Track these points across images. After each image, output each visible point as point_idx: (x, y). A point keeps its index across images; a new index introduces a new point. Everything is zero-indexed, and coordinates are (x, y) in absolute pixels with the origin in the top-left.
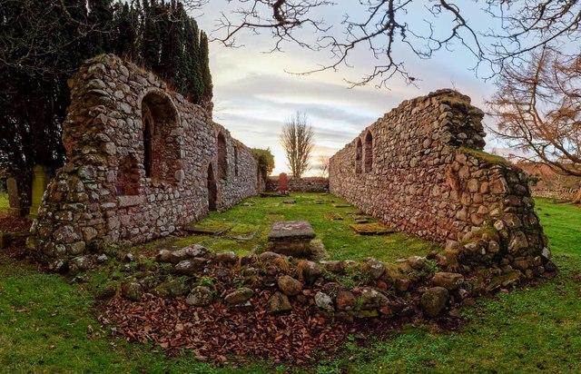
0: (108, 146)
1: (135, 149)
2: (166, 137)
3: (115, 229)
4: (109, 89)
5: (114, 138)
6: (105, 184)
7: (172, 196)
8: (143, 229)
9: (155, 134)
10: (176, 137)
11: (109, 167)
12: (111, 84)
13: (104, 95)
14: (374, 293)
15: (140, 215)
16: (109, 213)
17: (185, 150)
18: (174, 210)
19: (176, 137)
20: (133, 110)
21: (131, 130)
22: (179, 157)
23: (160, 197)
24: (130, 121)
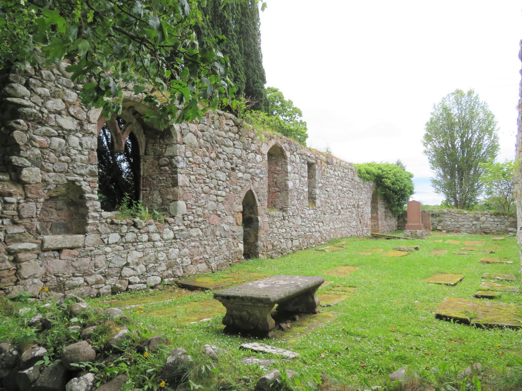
0: (25, 172)
1: (81, 175)
2: (159, 158)
3: (34, 276)
4: (36, 98)
5: (36, 162)
6: (17, 219)
7: (157, 237)
8: (90, 279)
9: (146, 154)
10: (172, 157)
11: (26, 198)
12: (40, 90)
13: (25, 106)
14: (124, 165)
15: (87, 260)
16: (21, 256)
17: (189, 175)
18: (162, 256)
19: (172, 157)
20: (81, 124)
21: (73, 151)
22: (175, 184)
23: (130, 237)
24: (74, 140)
